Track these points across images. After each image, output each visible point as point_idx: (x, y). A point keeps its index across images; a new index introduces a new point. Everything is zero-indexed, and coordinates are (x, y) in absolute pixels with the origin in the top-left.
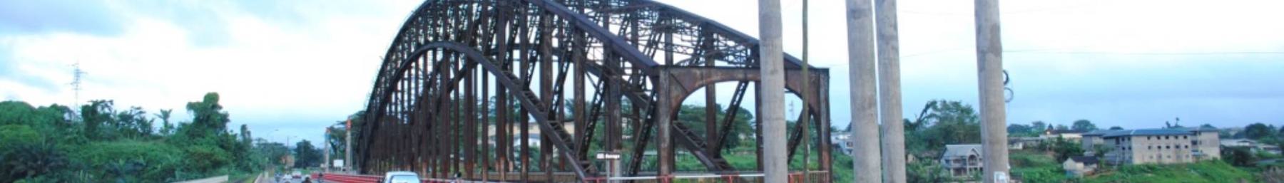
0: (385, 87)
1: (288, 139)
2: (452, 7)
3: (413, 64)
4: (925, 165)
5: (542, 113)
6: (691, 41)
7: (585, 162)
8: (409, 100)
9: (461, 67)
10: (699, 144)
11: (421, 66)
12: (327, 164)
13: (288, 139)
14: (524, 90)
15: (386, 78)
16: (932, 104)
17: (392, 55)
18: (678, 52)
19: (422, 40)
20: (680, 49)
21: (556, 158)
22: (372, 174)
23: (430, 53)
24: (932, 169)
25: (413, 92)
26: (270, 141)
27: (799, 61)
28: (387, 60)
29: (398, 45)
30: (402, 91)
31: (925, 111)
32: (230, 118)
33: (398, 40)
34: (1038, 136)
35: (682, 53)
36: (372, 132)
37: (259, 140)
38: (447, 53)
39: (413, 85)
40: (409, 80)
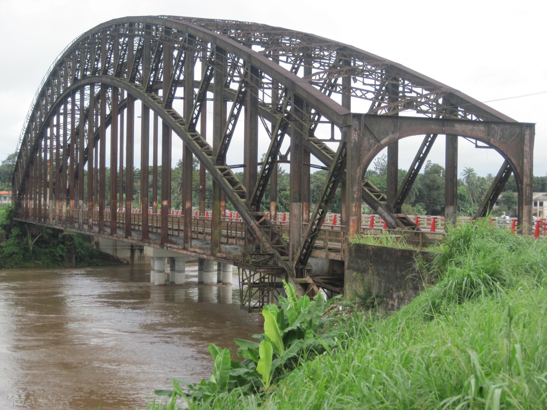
2: (111, 41)
3: (70, 99)
5: (209, 157)
6: (375, 85)
8: (65, 134)
9: (108, 112)
11: (78, 103)
17: (48, 90)
18: (356, 96)
19: (79, 75)
20: (359, 93)
25: (69, 127)
27: (337, 104)
28: (42, 95)
29: (54, 79)
30: (58, 126)
33: (54, 74)
35: (361, 97)
36: (24, 180)
38: (104, 87)
39: (69, 120)
40: (65, 114)
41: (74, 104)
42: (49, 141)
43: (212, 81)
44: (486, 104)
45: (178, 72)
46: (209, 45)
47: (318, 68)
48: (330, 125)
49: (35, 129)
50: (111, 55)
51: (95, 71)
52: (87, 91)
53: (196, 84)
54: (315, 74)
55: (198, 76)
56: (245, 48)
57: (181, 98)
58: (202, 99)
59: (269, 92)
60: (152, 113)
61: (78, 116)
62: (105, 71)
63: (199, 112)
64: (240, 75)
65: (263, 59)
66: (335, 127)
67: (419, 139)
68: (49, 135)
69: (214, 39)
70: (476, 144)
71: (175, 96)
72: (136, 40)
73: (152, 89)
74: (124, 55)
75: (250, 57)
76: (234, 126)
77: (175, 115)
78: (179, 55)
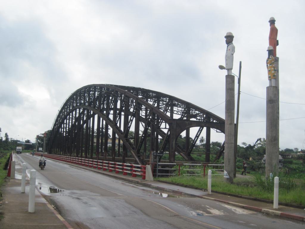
0: (58, 126)
1: (22, 139)
4: (256, 162)
6: (182, 110)
7: (139, 155)
9: (85, 119)
10: (182, 150)
11: (74, 115)
12: (36, 149)
13: (22, 139)
14: (115, 126)
15: (58, 122)
16: (260, 139)
21: (122, 152)
22: (53, 154)
23: (78, 110)
24: (259, 163)
25: (70, 124)
26: (36, 137)
29: (65, 106)
30: (66, 124)
31: (257, 142)
32: (38, 135)
34: (297, 153)
37: (11, 139)
41: (72, 116)
42: (62, 129)
43: (124, 109)
44: (209, 111)
45: (111, 104)
46: (123, 95)
47: (162, 104)
48: (165, 123)
49: (58, 124)
50: (87, 98)
51: (81, 104)
52: (78, 111)
53: (118, 109)
54: (161, 105)
55: (119, 106)
56: (136, 96)
57: (112, 114)
58: (120, 115)
59: (144, 112)
60: (101, 119)
61: (74, 120)
62: (84, 103)
63: (119, 119)
64: (134, 106)
65: (141, 100)
66: (167, 124)
67: (197, 128)
68: (63, 127)
69: (125, 93)
70: (217, 131)
71: (110, 113)
72: (96, 93)
73: (102, 111)
74: (92, 98)
75: (137, 99)
76: (131, 124)
77: (109, 119)
78: (112, 98)
